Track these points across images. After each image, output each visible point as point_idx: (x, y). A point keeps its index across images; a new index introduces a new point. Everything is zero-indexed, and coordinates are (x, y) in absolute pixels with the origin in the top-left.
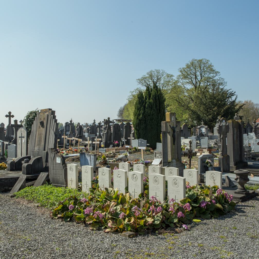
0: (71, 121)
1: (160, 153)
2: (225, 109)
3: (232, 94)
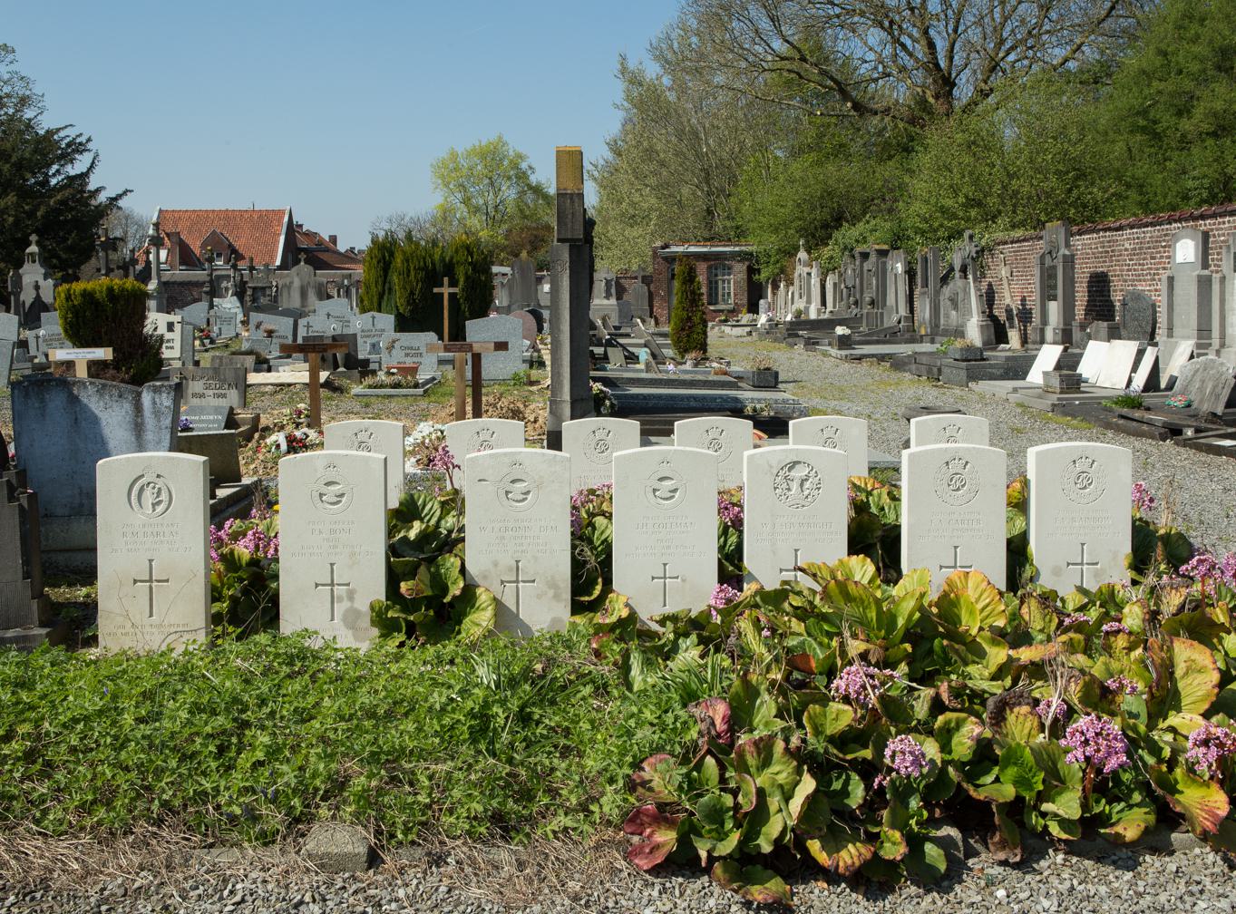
0: (500, 138)
1: (211, 372)
2: (51, 203)
3: (77, 148)
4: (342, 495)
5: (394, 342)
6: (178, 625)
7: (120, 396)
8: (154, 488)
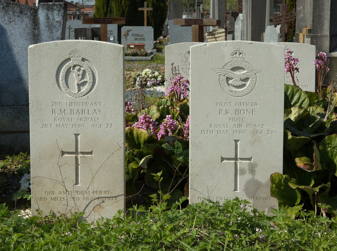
4: (247, 79)
5: (128, 31)
6: (101, 192)
7: (21, 12)
8: (79, 70)
